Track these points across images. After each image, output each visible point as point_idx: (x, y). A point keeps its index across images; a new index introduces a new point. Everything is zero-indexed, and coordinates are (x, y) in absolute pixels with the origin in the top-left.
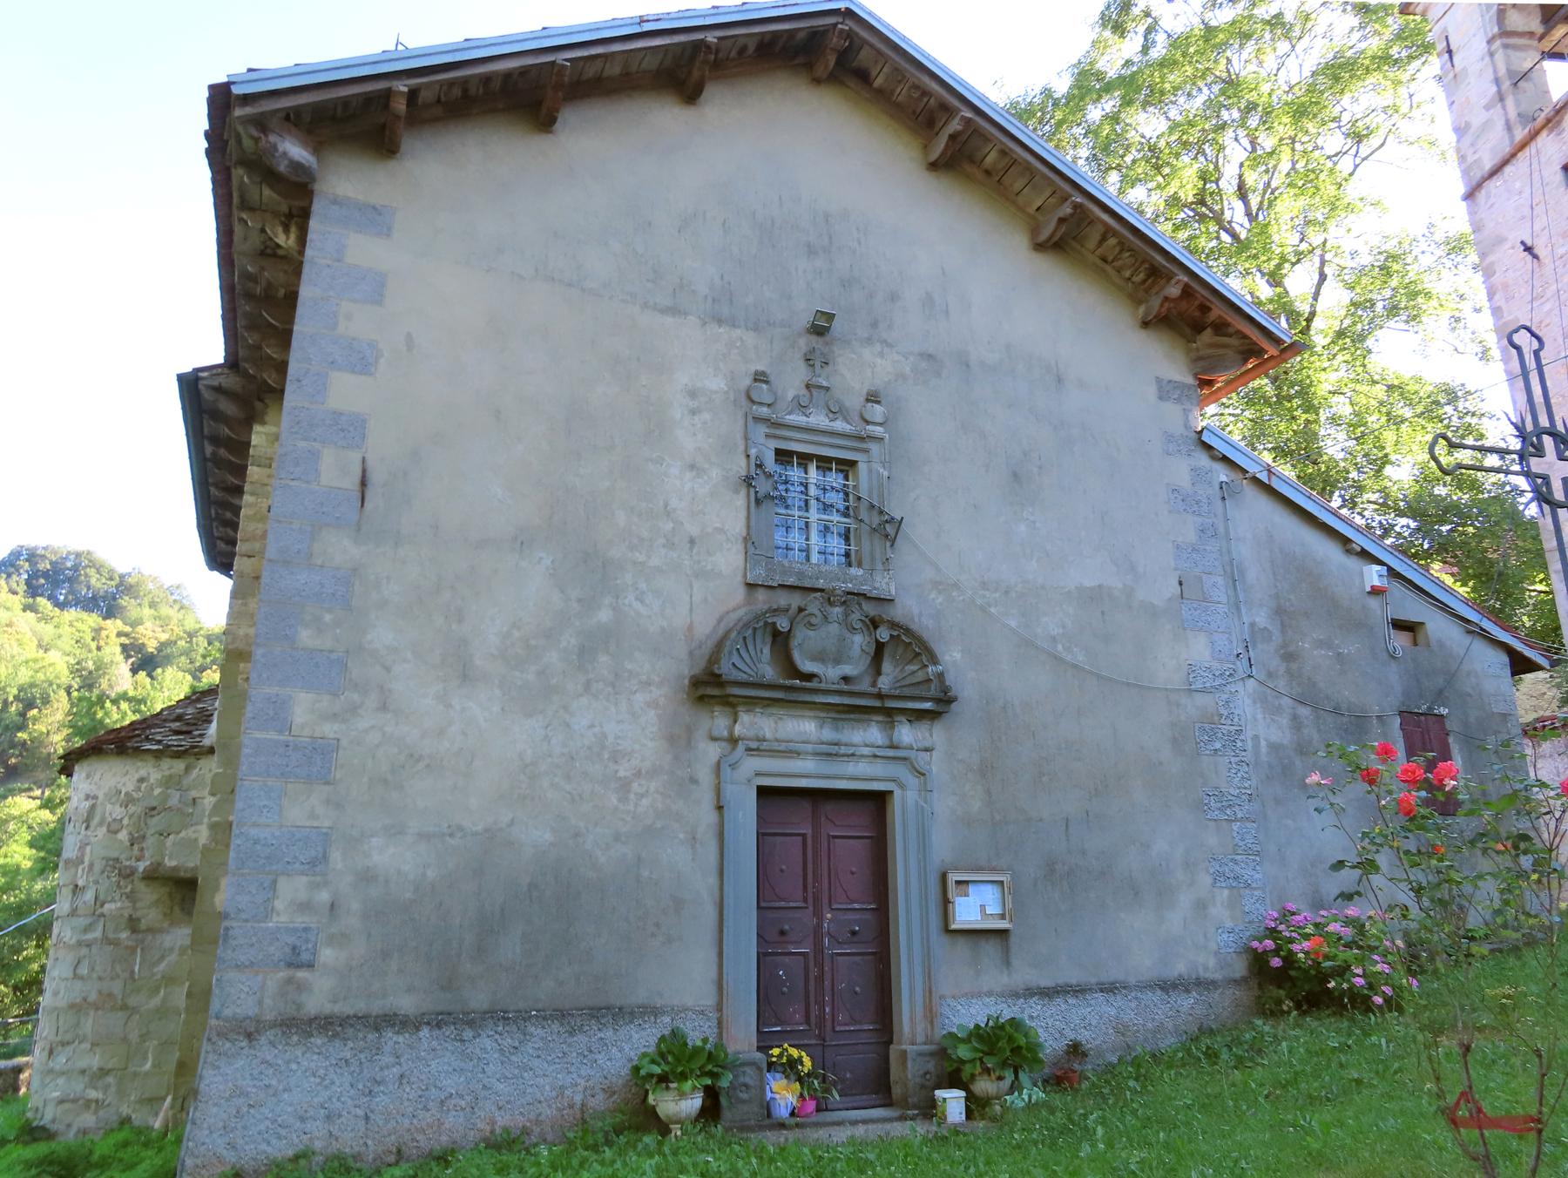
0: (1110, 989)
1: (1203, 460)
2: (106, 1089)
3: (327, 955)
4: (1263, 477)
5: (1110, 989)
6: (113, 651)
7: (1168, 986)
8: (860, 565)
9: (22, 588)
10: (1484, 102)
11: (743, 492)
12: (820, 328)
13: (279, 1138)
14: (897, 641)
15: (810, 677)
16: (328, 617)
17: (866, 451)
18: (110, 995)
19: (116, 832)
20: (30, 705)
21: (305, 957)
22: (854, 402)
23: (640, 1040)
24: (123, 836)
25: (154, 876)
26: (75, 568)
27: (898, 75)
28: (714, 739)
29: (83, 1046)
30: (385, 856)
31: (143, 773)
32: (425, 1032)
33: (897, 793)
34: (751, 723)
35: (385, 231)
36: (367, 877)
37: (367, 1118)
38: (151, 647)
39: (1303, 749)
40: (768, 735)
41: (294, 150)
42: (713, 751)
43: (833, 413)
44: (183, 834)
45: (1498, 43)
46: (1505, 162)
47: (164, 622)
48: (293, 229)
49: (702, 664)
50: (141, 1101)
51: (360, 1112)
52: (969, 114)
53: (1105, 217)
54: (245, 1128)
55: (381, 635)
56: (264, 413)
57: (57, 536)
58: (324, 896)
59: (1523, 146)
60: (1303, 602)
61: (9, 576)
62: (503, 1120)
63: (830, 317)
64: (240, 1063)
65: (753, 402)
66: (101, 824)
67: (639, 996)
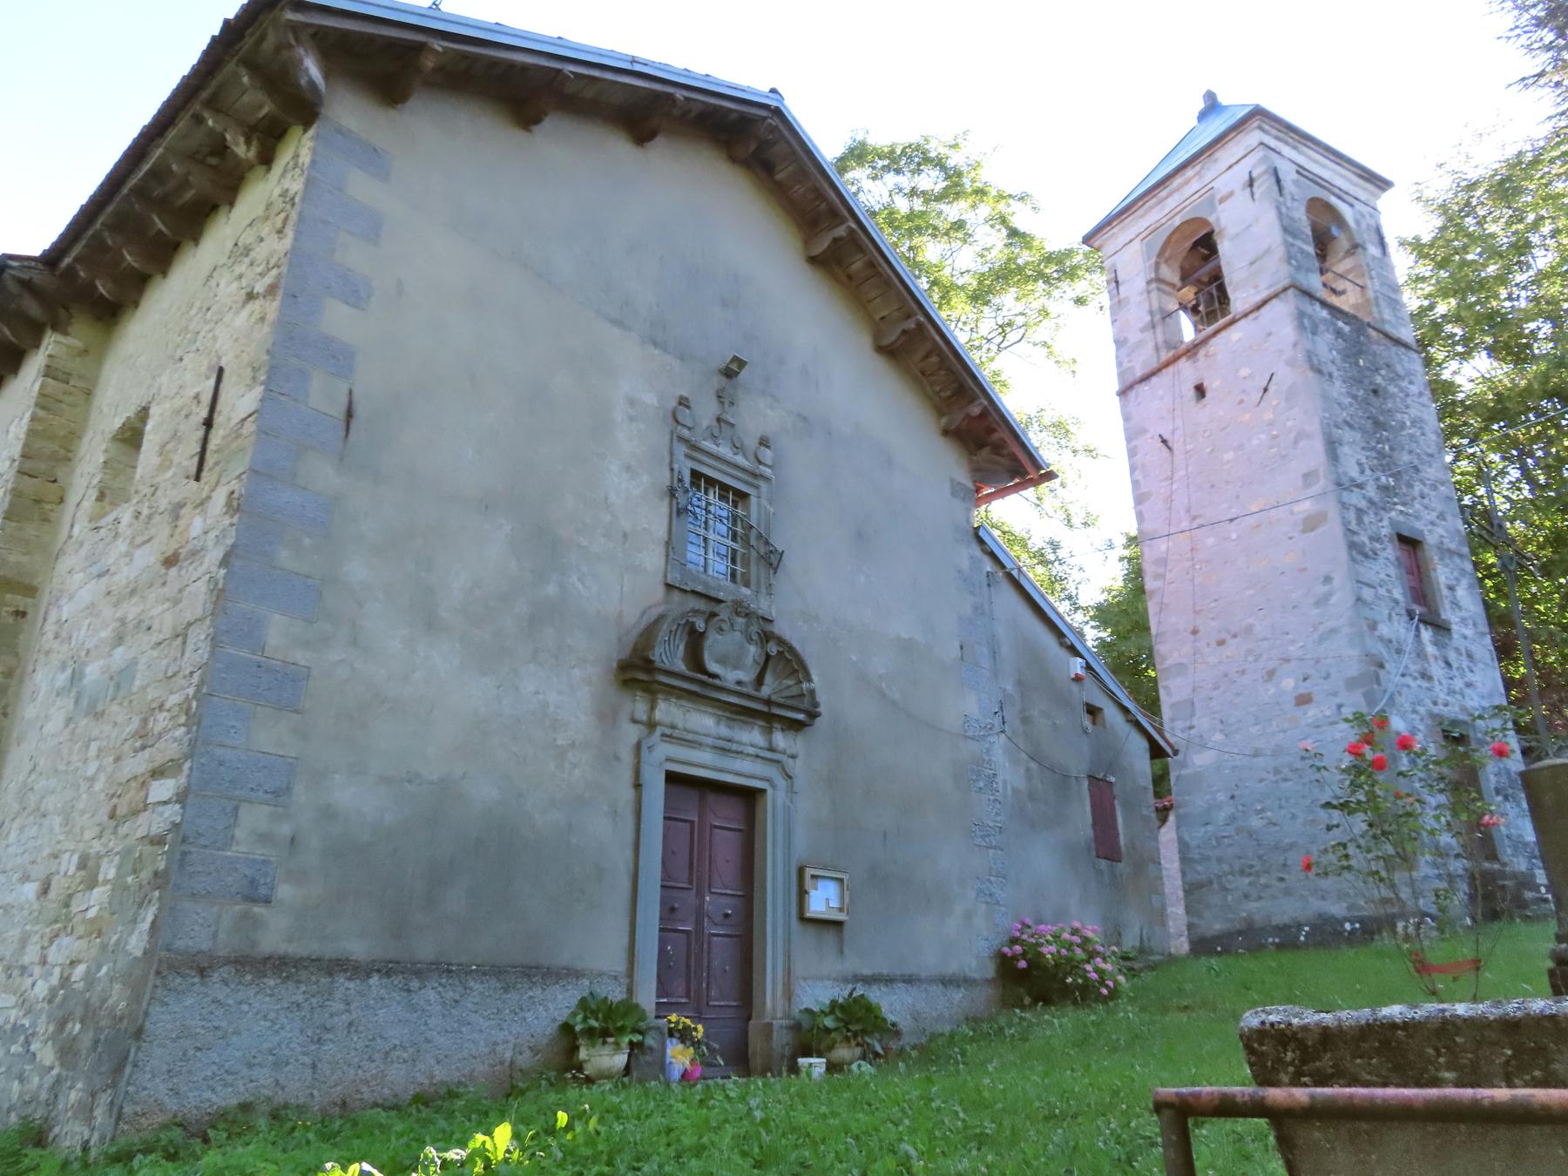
0: (909, 980)
1: (976, 551)
3: (285, 892)
4: (1015, 573)
5: (909, 980)
7: (947, 982)
8: (747, 585)
10: (1140, 325)
11: (666, 502)
12: (732, 371)
14: (783, 659)
15: (715, 676)
17: (757, 487)
21: (263, 891)
22: (751, 443)
23: (560, 1004)
27: (802, 174)
28: (635, 721)
32: (375, 980)
33: (770, 792)
34: (667, 711)
36: (328, 813)
37: (314, 1066)
39: (1032, 796)
40: (680, 725)
41: (312, 68)
42: (632, 733)
43: (737, 448)
45: (1154, 285)
46: (1153, 374)
48: (255, 143)
49: (635, 649)
51: (307, 1060)
52: (854, 226)
53: (937, 338)
54: (190, 1072)
55: (357, 570)
56: (69, 324)
58: (285, 829)
59: (1167, 364)
60: (1035, 682)
62: (440, 1074)
63: (742, 364)
64: (189, 1001)
65: (677, 422)
67: (564, 959)
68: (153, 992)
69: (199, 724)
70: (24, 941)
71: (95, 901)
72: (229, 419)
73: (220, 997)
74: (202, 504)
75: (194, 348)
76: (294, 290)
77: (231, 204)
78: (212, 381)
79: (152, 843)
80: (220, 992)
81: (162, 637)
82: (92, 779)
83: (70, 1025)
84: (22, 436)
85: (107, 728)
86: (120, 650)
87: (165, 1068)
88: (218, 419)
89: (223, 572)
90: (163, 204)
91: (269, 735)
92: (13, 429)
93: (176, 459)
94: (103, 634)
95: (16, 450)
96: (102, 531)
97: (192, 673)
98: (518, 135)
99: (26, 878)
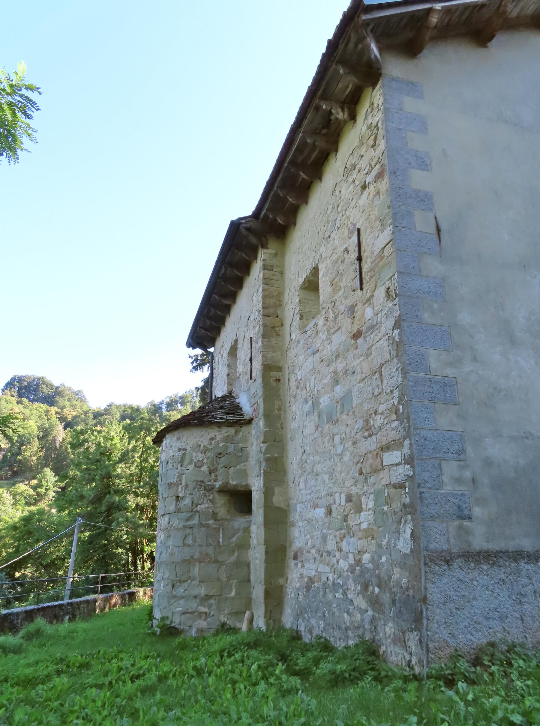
2: (210, 607)
3: (477, 511)
6: (54, 419)
9: (16, 394)
13: (477, 631)
16: (436, 306)
18: (207, 554)
19: (200, 467)
20: (22, 445)
21: (466, 512)
24: (205, 468)
25: (225, 491)
26: (37, 385)
29: (194, 582)
30: (496, 450)
31: (212, 435)
35: (420, 96)
36: (488, 463)
37: (522, 619)
38: (69, 418)
44: (238, 467)
47: (74, 407)
48: (346, 110)
50: (231, 614)
55: (465, 317)
56: (267, 244)
57: (30, 370)
58: (468, 474)
61: (11, 389)
64: (445, 580)
66: (191, 462)
68: (426, 576)
69: (408, 418)
70: (324, 538)
71: (365, 519)
72: (373, 252)
73: (461, 577)
74: (368, 300)
75: (336, 228)
76: (394, 168)
77: (336, 151)
78: (355, 238)
79: (395, 487)
80: (460, 574)
81: (364, 376)
82: (341, 455)
83: (371, 588)
84: (261, 299)
85: (343, 428)
86: (338, 388)
87: (443, 620)
88: (364, 256)
89: (396, 332)
90: (302, 166)
91: (445, 420)
92: (254, 298)
93: (342, 284)
94: (325, 381)
95: (260, 306)
96: (308, 333)
97: (392, 391)
98: (481, 52)
99: (315, 506)
